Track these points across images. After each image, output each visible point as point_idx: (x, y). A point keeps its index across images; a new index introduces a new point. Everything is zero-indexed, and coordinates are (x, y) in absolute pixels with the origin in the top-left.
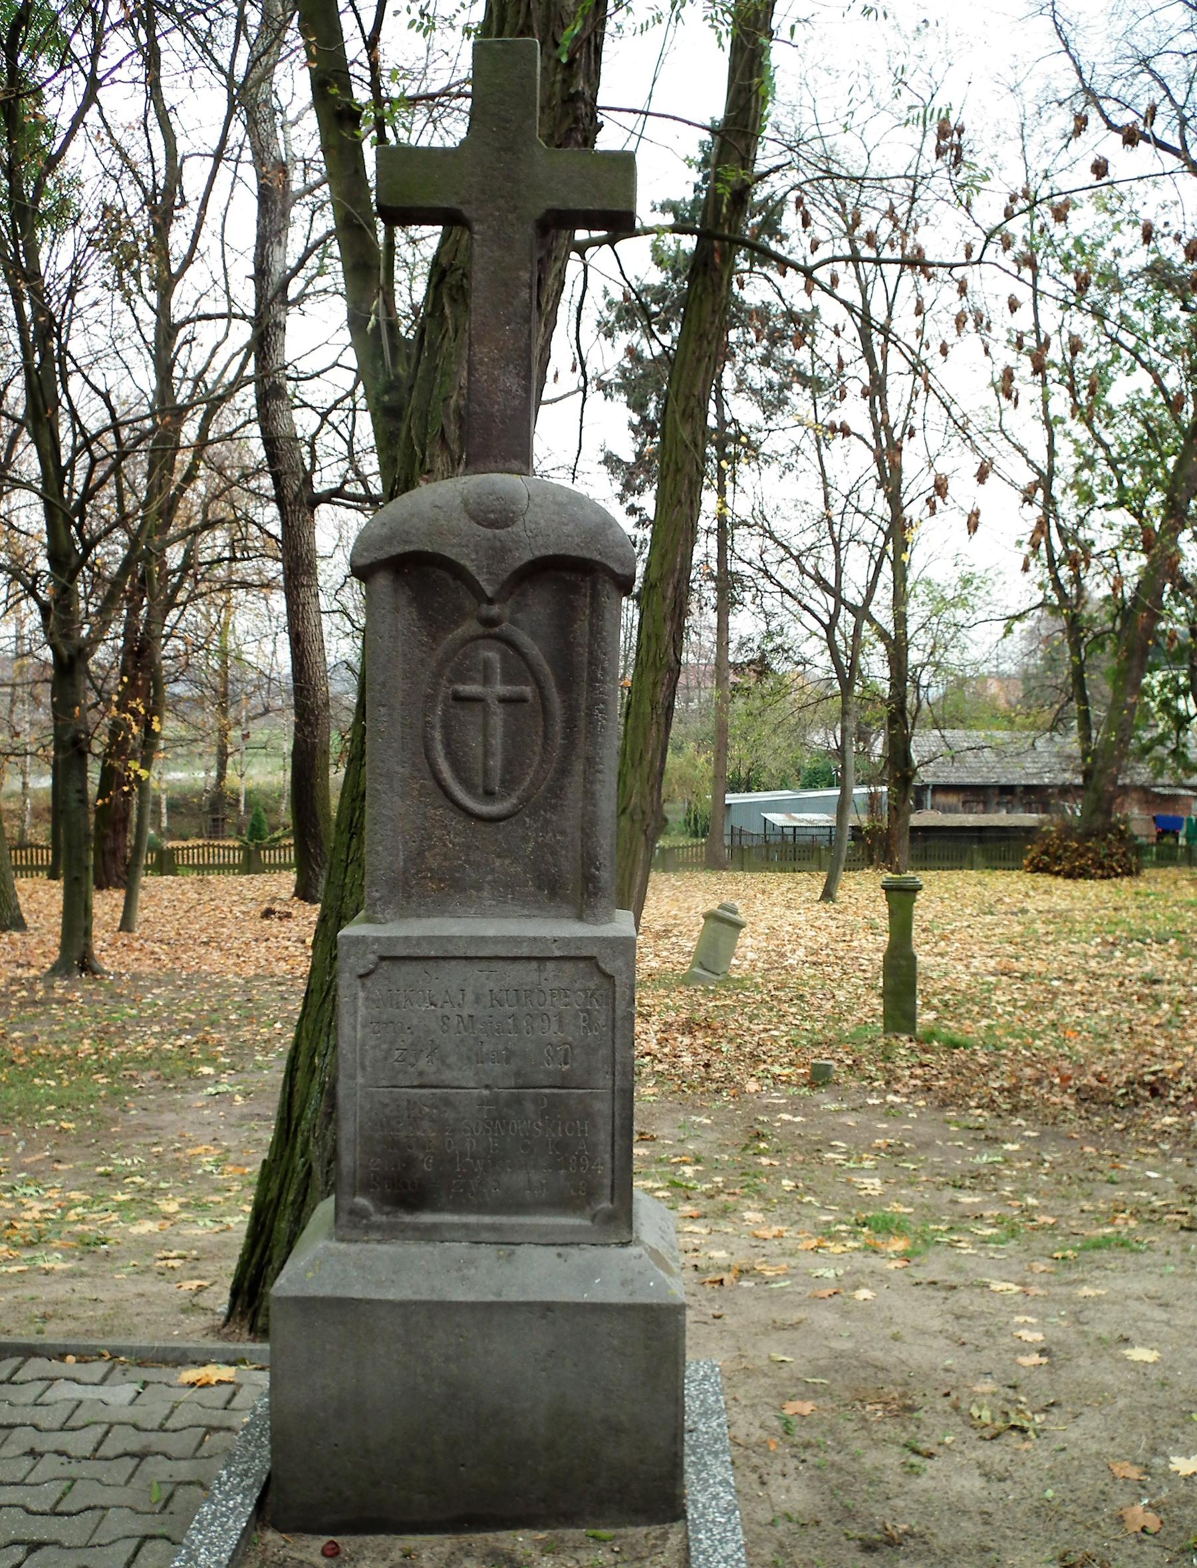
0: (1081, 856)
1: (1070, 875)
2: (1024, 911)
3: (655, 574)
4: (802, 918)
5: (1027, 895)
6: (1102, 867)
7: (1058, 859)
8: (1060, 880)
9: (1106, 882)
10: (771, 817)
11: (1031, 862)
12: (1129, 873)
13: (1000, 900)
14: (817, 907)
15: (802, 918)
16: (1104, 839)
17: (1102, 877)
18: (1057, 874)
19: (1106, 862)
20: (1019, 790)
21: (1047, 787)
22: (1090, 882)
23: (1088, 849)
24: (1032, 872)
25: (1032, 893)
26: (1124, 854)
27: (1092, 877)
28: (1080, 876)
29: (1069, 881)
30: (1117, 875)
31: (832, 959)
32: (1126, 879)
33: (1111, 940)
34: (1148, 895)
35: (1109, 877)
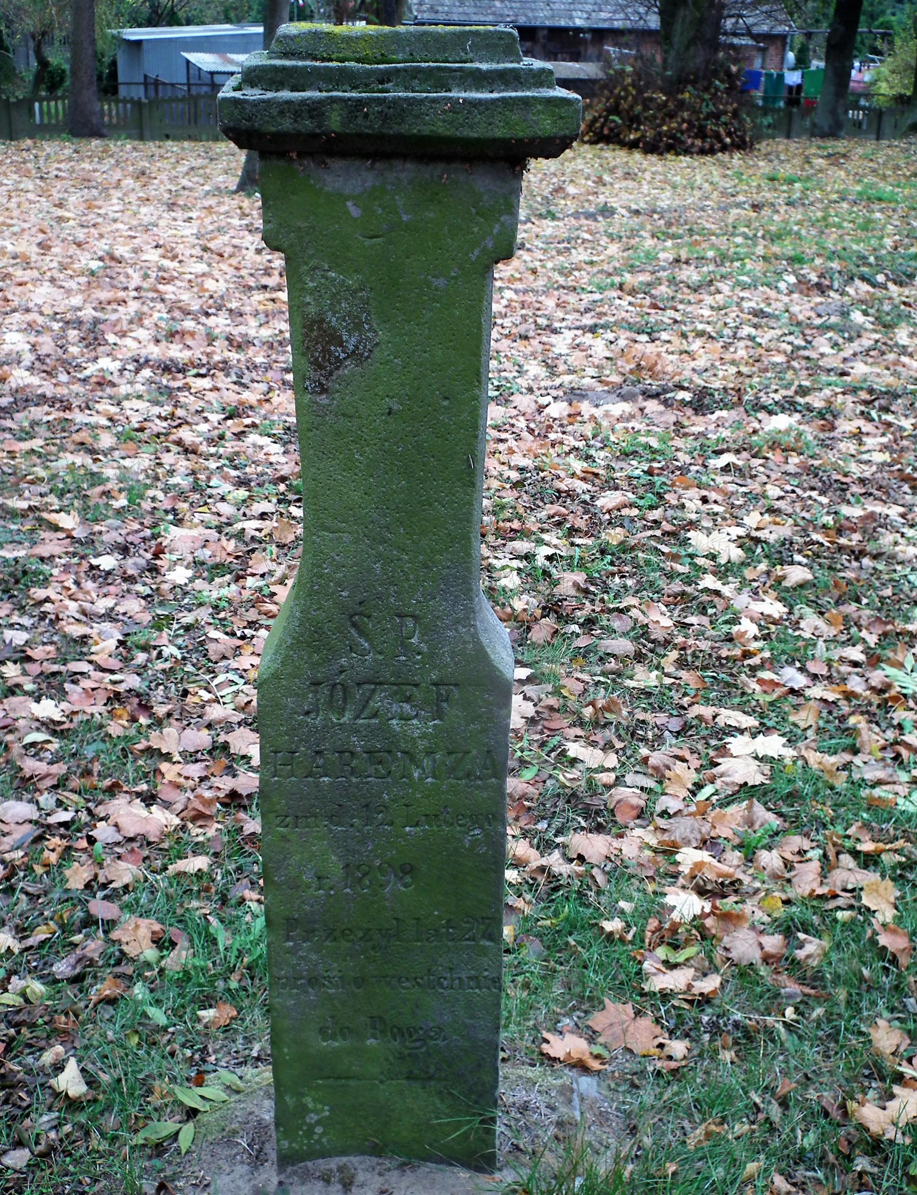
0: (671, 116)
1: (652, 148)
2: (607, 211)
3: (322, 85)
4: (189, 231)
5: (600, 181)
6: (702, 134)
7: (633, 121)
8: (637, 156)
9: (708, 158)
10: (195, 58)
11: (590, 127)
12: (742, 145)
13: (559, 190)
14: (230, 204)
15: (189, 231)
16: (706, 89)
17: (703, 152)
18: (632, 146)
19: (710, 126)
20: (541, 34)
21: (578, 30)
22: (685, 160)
23: (681, 105)
24: (592, 142)
25: (606, 178)
26: (735, 114)
27: (687, 152)
28: (670, 148)
29: (653, 158)
30: (724, 148)
31: (221, 351)
32: (737, 155)
33: (814, 278)
34: (791, 182)
35: (711, 151)
